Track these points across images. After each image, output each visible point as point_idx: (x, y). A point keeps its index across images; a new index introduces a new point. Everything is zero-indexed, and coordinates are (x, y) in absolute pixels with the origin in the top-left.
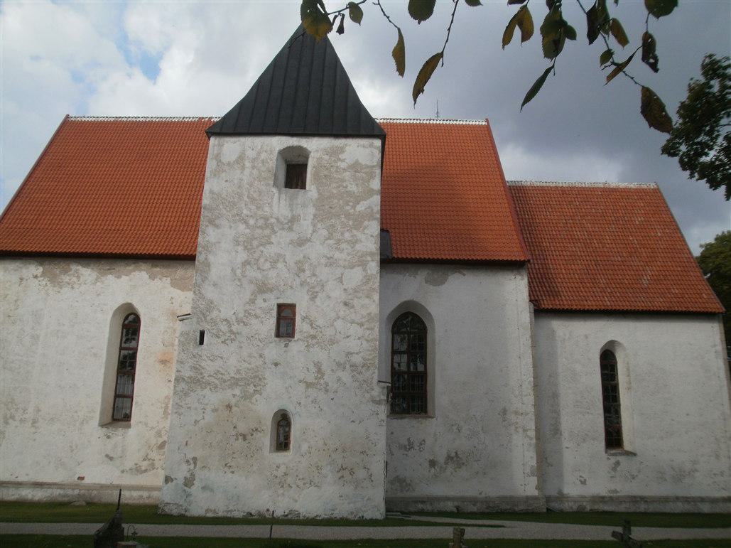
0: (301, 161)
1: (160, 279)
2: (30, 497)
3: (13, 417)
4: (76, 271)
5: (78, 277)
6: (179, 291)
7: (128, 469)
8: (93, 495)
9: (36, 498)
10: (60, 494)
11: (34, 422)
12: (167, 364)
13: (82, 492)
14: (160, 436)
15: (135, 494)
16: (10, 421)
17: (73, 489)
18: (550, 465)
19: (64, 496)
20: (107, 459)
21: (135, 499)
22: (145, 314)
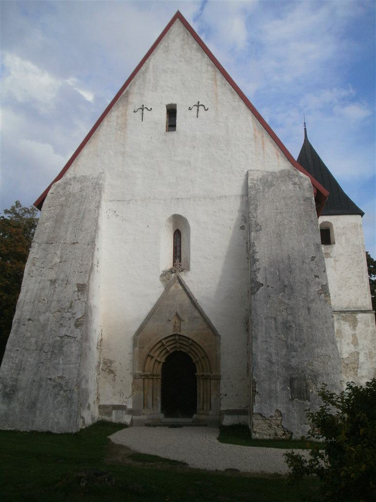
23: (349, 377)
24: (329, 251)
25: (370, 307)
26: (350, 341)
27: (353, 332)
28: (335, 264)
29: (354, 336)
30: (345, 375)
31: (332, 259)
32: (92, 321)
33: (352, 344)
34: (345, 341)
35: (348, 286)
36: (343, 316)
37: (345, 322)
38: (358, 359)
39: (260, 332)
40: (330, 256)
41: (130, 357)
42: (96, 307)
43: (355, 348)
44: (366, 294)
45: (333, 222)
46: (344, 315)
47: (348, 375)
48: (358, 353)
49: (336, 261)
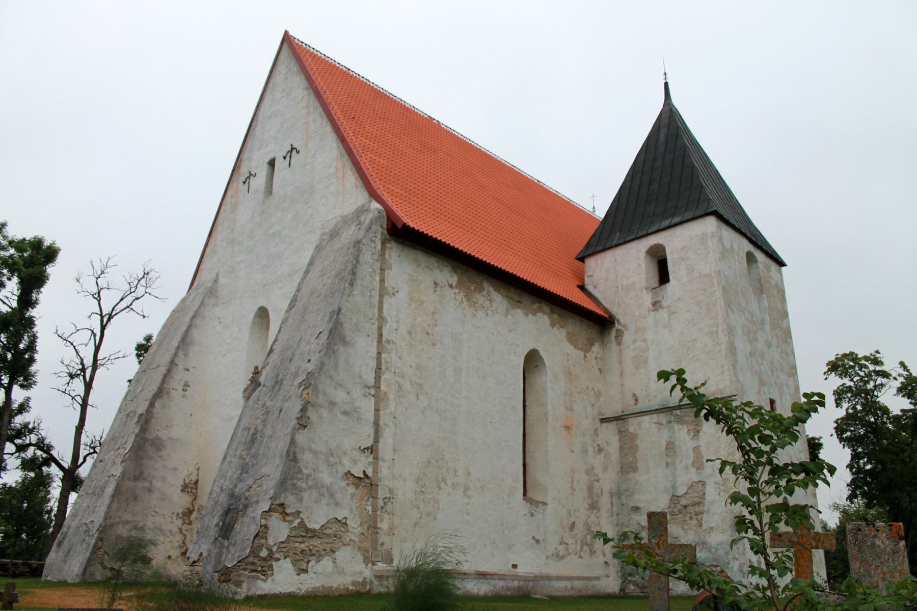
0: (664, 258)
1: (558, 329)
2: (475, 591)
3: (444, 480)
4: (489, 292)
5: (491, 301)
6: (908, 570)
7: (550, 555)
8: (530, 587)
9: (482, 593)
10: (503, 587)
11: (466, 489)
12: (701, 504)
13: (521, 582)
14: (570, 516)
15: (562, 584)
16: (443, 485)
17: (513, 580)
18: (345, 342)
19: (508, 589)
20: (533, 542)
21: (562, 591)
22: (523, 354)
23: (689, 531)
24: (660, 298)
25: (88, 406)
26: (689, 462)
27: (694, 444)
28: (670, 320)
29: (696, 449)
30: (682, 527)
31: (665, 310)
32: (580, 591)
33: (693, 466)
34: (681, 461)
35: (691, 356)
36: (677, 415)
37: (680, 426)
38: (704, 494)
39: (300, 369)
40: (661, 307)
41: (264, 186)
42: (35, 236)
43: (698, 474)
44: (723, 366)
45: (665, 244)
46: (678, 412)
47: (686, 527)
48: (704, 484)
49: (671, 313)
